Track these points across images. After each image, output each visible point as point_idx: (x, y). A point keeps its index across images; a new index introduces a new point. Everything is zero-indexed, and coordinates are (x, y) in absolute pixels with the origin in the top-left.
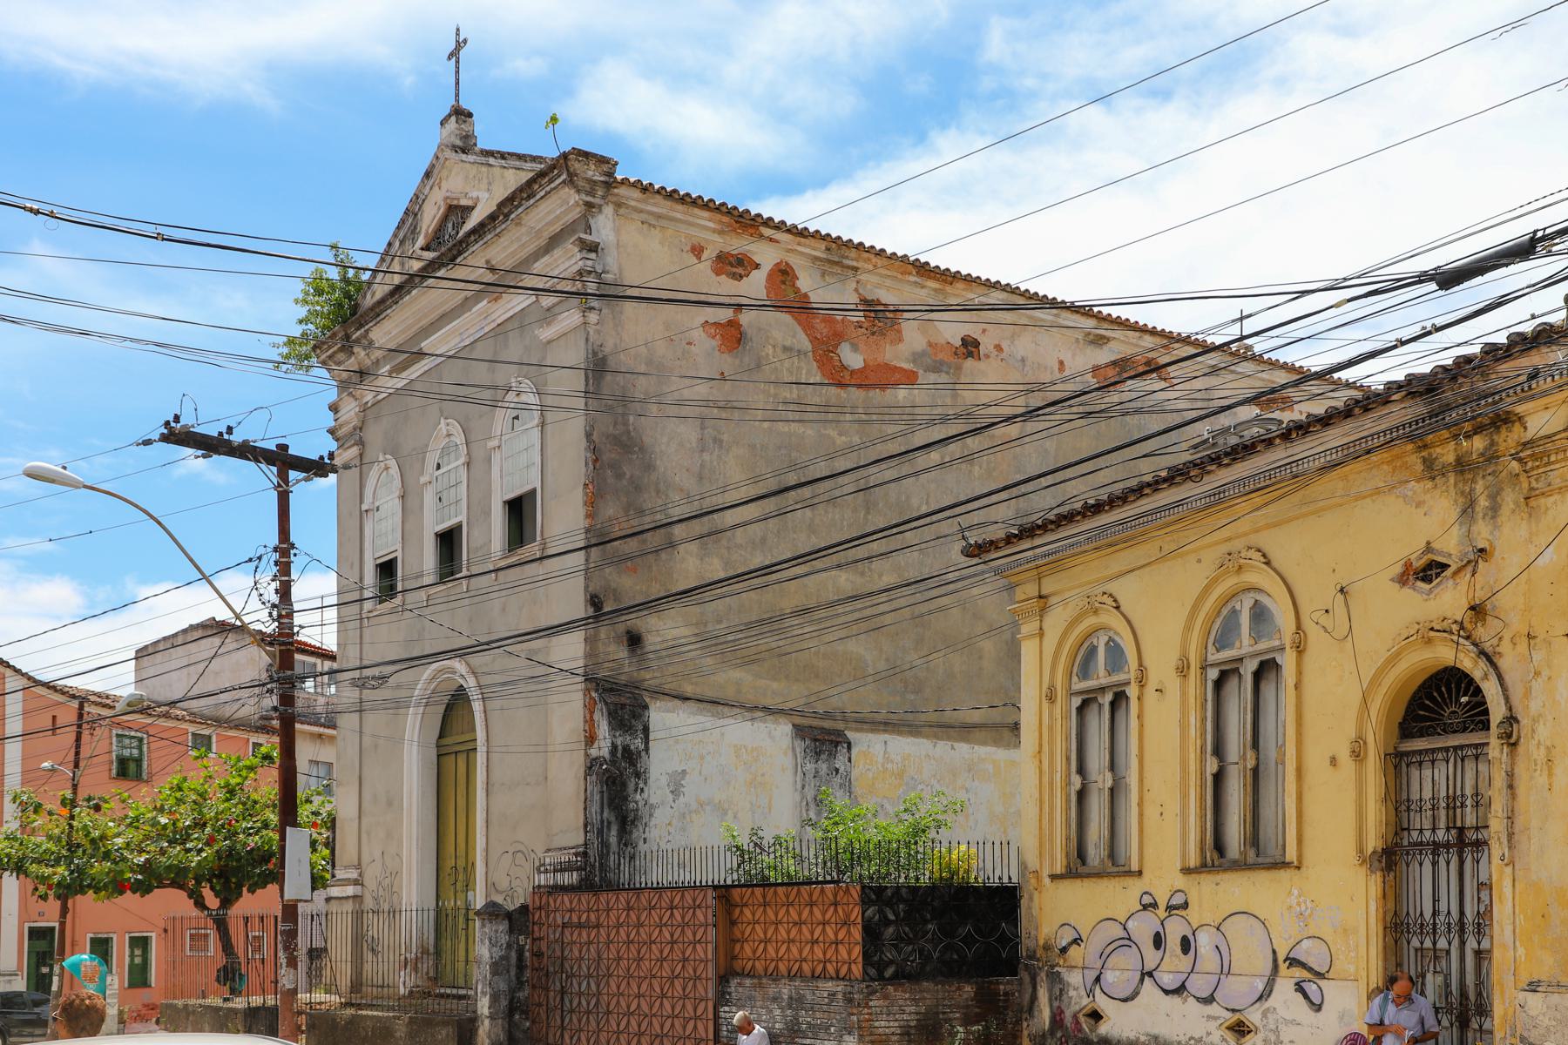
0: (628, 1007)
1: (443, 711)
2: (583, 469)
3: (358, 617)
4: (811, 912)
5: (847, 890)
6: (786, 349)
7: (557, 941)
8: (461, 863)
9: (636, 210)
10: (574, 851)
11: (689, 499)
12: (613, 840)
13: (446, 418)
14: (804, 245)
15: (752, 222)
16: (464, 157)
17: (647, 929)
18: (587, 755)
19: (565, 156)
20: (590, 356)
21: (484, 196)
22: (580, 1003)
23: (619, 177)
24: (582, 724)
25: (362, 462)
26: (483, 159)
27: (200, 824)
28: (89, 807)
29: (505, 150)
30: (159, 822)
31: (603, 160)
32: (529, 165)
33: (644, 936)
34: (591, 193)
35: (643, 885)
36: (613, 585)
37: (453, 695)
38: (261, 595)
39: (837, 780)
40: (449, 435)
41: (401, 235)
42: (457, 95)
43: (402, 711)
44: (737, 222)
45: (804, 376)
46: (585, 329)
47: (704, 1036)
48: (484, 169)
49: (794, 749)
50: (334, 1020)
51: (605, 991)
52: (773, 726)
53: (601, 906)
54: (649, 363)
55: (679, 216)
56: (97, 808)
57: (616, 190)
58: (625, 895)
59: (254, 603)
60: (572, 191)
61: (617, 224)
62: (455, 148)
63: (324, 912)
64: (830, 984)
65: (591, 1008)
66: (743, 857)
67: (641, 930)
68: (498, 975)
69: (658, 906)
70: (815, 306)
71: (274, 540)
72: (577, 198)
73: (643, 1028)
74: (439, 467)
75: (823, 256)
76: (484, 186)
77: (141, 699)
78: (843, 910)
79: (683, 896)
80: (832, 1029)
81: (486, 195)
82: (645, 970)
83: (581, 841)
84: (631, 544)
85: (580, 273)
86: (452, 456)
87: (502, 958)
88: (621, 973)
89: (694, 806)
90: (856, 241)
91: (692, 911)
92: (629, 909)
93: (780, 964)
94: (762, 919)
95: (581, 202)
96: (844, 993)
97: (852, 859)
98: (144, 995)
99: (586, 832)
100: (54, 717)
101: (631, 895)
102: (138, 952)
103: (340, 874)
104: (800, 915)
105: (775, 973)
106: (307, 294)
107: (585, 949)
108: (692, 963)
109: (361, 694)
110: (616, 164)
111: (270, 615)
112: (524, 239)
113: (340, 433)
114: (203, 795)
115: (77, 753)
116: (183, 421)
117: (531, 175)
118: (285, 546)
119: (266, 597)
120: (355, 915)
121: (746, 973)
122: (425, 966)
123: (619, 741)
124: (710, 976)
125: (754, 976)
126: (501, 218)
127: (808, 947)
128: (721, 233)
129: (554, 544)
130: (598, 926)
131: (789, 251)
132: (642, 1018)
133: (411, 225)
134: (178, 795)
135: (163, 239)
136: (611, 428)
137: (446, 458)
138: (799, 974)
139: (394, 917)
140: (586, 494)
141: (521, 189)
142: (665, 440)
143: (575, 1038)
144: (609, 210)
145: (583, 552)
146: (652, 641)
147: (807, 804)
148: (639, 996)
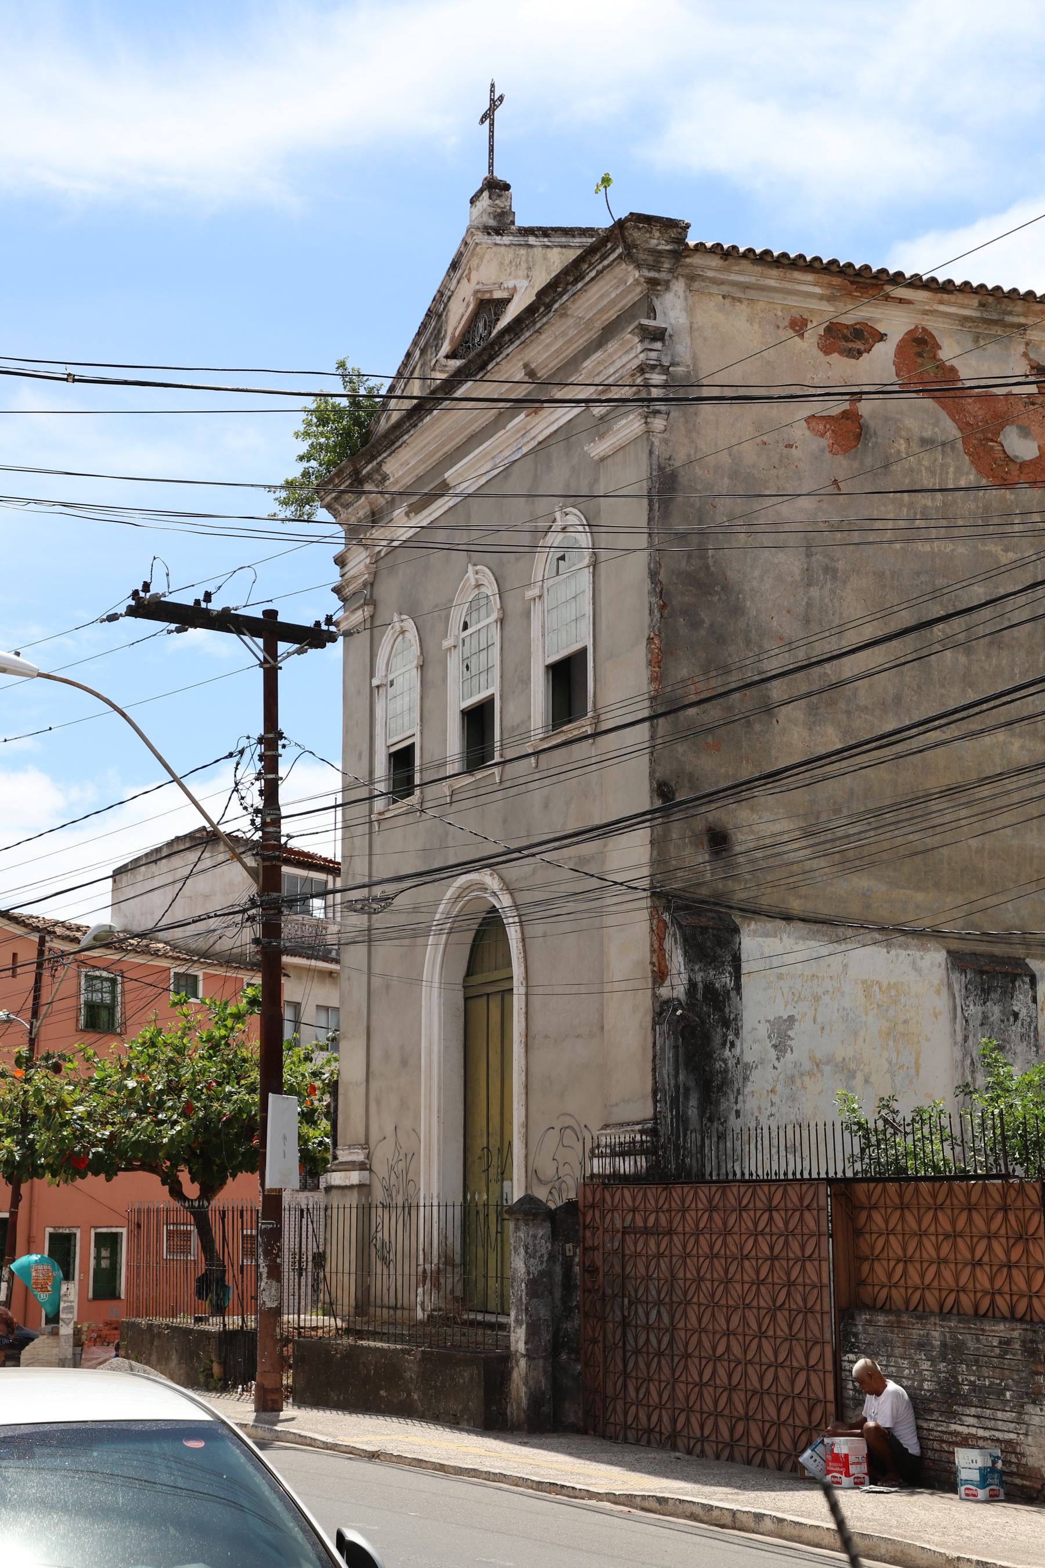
0: (714, 1349)
1: (470, 940)
2: (647, 619)
3: (367, 819)
4: (970, 1219)
5: (1021, 1189)
6: (924, 441)
7: (615, 1252)
8: (494, 1143)
9: (714, 281)
10: (639, 1127)
11: (790, 645)
12: (693, 1112)
13: (475, 565)
14: (949, 304)
15: (874, 281)
16: (498, 239)
17: (736, 1237)
18: (655, 996)
19: (620, 224)
20: (655, 473)
21: (522, 284)
22: (648, 1340)
23: (691, 242)
24: (648, 955)
25: (373, 626)
26: (521, 240)
27: (173, 1089)
28: (47, 1067)
29: (548, 226)
30: (126, 1086)
31: (669, 224)
32: (577, 241)
33: (734, 1249)
34: (655, 267)
35: (731, 1177)
36: (688, 768)
37: (484, 919)
38: (243, 798)
39: (1016, 1029)
40: (478, 586)
41: (422, 343)
42: (491, 165)
43: (420, 941)
44: (852, 283)
45: (951, 476)
46: (648, 439)
47: (821, 1396)
48: (522, 251)
49: (950, 986)
50: (328, 1352)
51: (681, 1325)
52: (918, 954)
53: (673, 1204)
54: (734, 475)
55: (772, 283)
56: (57, 1069)
57: (688, 260)
58: (706, 1191)
59: (235, 808)
60: (631, 268)
61: (690, 302)
62: (487, 230)
63: (323, 1206)
64: (1002, 1327)
65: (663, 1347)
66: (868, 1139)
67: (729, 1239)
68: (537, 1297)
69: (751, 1206)
70: (968, 384)
71: (258, 729)
72: (637, 274)
73: (735, 1380)
74: (466, 627)
75: (977, 314)
76: (522, 272)
77: (110, 930)
78: (1016, 1216)
79: (785, 1192)
80: (1008, 1394)
81: (525, 283)
82: (736, 1299)
83: (649, 1113)
84: (712, 712)
85: (642, 369)
86: (483, 611)
87: (542, 1273)
88: (703, 1300)
89: (807, 1065)
90: (1022, 290)
91: (798, 1214)
92: (712, 1209)
93: (927, 1293)
94: (899, 1228)
95: (643, 280)
96: (1024, 1342)
97: (1026, 1147)
98: (113, 1310)
99: (655, 1102)
100: (15, 955)
101: (713, 1189)
102: (105, 1253)
103: (343, 1156)
104: (953, 1223)
105: (920, 1308)
106: (309, 424)
107: (653, 1263)
108: (801, 1289)
109: (369, 920)
110: (688, 226)
111: (253, 822)
112: (572, 333)
113: (348, 591)
114: (180, 1051)
115: (36, 998)
116: (154, 590)
117: (579, 252)
118: (271, 736)
119: (248, 802)
120: (360, 1210)
121: (879, 1304)
122: (449, 1281)
123: (699, 977)
124: (826, 1308)
125: (889, 1311)
126: (542, 310)
127: (968, 1271)
128: (830, 299)
129: (609, 716)
130: (670, 1232)
131: (926, 313)
132: (733, 1365)
133: (434, 328)
134: (151, 1051)
135: (74, 381)
136: (684, 563)
137: (475, 615)
138: (955, 1311)
139: (410, 1214)
140: (650, 651)
141: (566, 272)
142: (757, 573)
143: (643, 1391)
144: (679, 286)
145: (646, 725)
146: (743, 841)
147: (972, 1063)
148: (728, 1333)
